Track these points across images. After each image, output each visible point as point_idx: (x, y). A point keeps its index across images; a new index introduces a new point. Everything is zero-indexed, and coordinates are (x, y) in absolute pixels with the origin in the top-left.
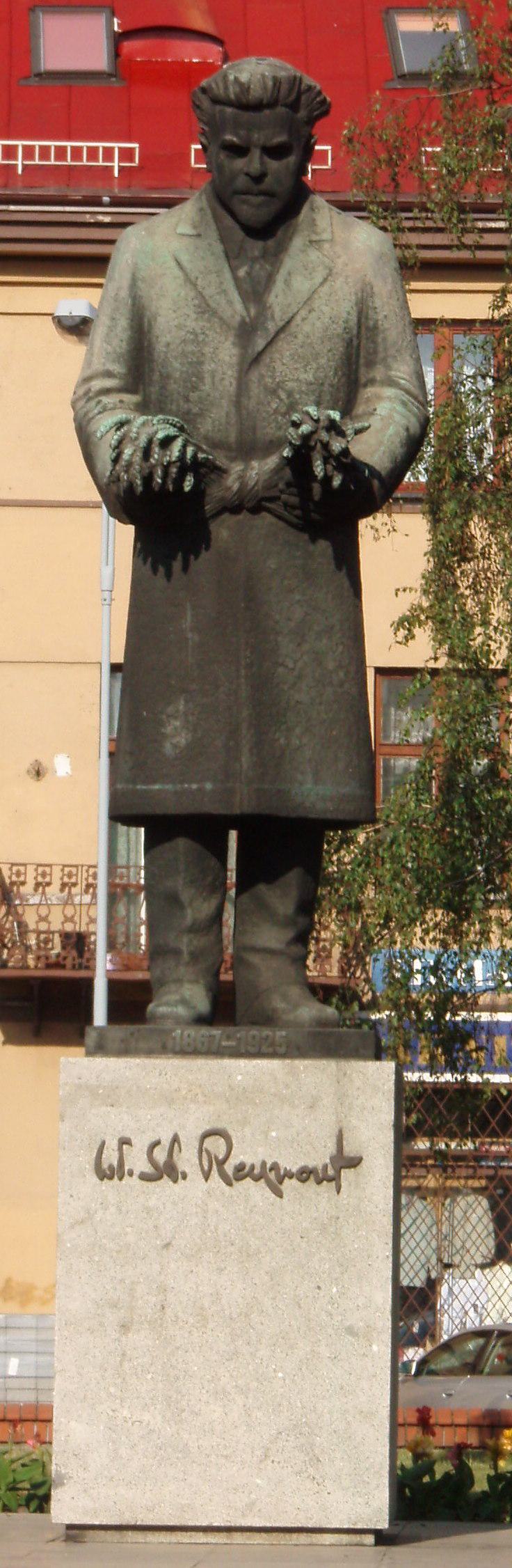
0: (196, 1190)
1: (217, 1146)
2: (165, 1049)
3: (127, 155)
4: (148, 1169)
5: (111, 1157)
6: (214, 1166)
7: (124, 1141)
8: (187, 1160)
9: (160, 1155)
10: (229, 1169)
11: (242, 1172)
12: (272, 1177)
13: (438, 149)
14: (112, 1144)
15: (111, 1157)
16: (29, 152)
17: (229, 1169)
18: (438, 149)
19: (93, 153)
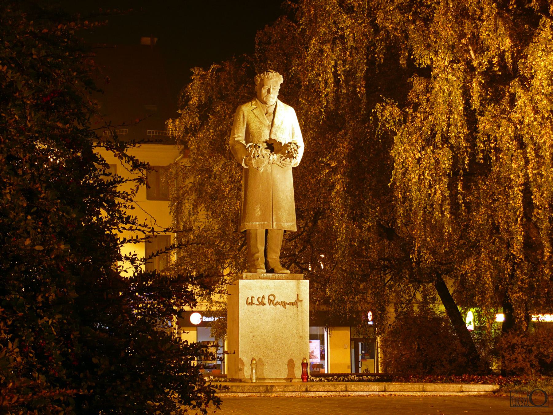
0: (268, 307)
1: (272, 298)
2: (260, 278)
3: (126, 131)
4: (258, 303)
5: (250, 301)
6: (270, 302)
7: (252, 297)
8: (266, 301)
9: (260, 300)
10: (275, 302)
11: (277, 303)
12: (284, 304)
13: (379, 339)
14: (250, 298)
15: (250, 301)
16: (153, 132)
17: (275, 302)
18: (379, 339)
19: (159, 133)
